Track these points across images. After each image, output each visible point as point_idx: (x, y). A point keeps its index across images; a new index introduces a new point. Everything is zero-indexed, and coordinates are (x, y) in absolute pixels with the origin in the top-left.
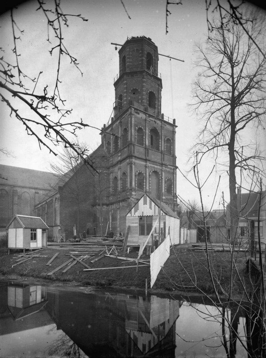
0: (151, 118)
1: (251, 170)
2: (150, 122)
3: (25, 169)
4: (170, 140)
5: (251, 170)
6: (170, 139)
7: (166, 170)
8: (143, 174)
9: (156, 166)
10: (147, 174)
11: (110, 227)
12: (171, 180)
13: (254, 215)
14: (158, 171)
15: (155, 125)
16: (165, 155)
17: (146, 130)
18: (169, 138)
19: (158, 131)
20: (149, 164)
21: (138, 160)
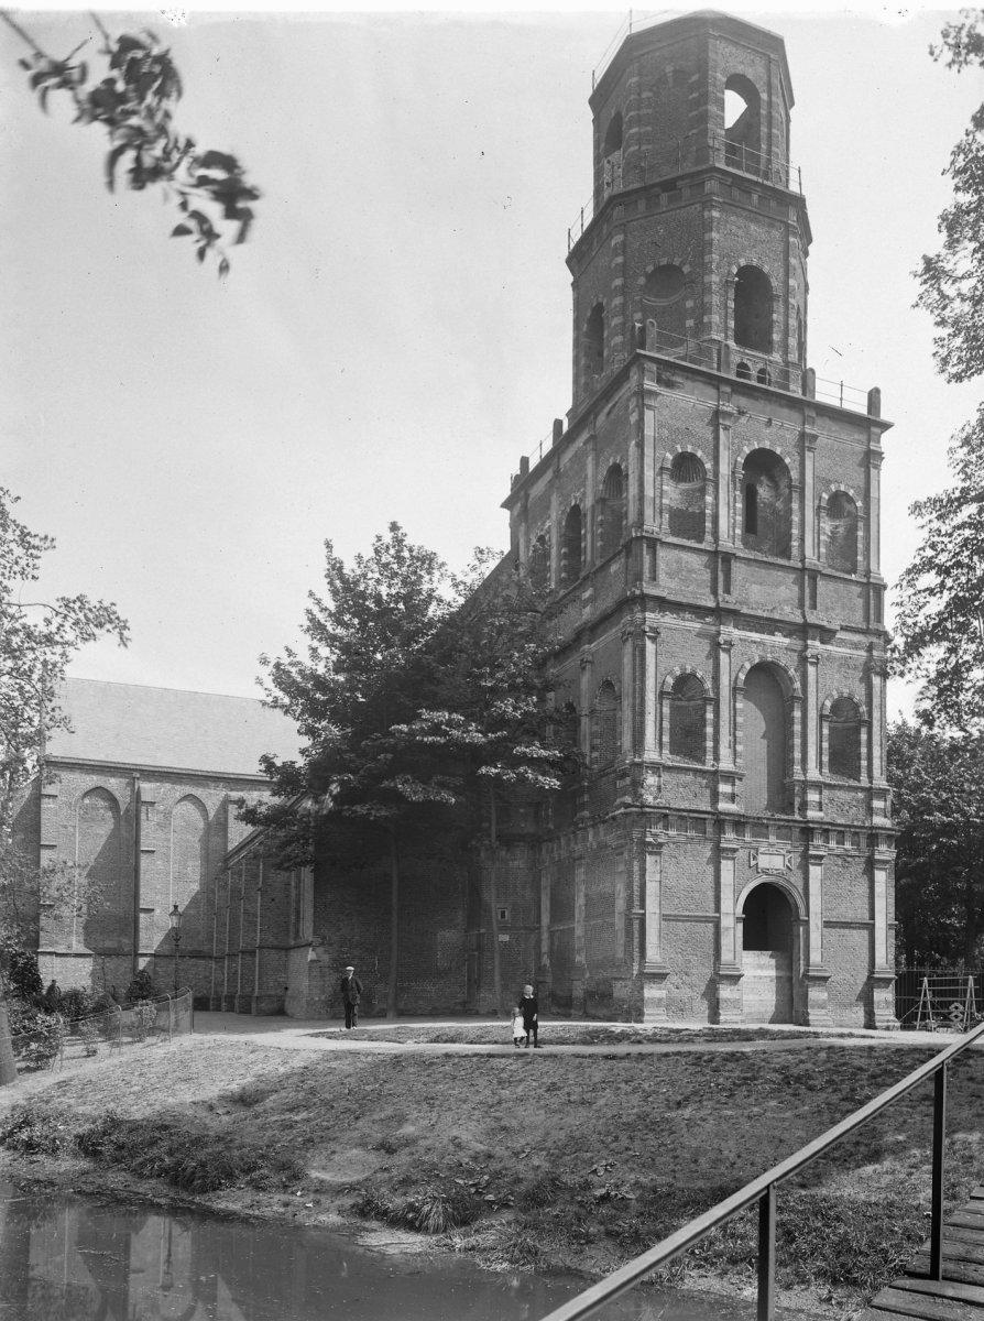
6: (851, 492)
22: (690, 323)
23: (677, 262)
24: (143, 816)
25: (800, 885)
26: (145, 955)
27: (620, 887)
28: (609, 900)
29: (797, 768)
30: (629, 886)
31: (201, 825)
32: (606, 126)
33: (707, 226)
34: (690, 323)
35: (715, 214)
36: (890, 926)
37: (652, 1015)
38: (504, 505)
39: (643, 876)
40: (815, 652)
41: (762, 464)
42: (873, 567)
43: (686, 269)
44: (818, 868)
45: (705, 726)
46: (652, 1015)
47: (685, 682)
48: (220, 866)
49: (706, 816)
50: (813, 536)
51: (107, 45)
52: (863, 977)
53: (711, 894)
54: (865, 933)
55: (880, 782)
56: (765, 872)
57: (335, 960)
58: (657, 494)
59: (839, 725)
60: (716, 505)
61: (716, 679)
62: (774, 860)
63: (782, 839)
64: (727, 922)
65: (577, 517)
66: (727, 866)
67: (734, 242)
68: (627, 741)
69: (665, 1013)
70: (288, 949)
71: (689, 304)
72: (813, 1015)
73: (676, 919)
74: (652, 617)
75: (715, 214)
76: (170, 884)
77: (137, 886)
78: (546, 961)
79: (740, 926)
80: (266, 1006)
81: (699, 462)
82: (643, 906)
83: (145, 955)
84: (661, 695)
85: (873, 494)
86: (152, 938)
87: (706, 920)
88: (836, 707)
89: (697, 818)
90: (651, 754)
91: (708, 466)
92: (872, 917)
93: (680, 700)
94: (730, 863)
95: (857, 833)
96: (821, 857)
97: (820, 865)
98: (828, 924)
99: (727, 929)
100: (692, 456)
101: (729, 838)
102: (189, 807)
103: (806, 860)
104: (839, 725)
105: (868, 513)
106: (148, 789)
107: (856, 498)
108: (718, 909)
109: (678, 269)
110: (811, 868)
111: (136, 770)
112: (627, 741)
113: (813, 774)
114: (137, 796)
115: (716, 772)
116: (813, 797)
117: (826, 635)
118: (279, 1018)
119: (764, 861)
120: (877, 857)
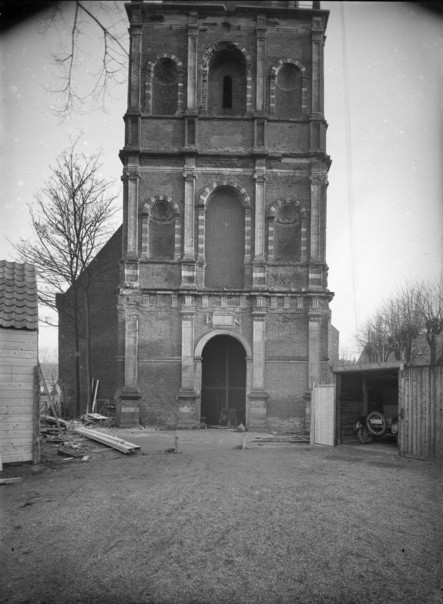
0: (210, 20)
1: (94, 234)
2: (204, 30)
3: (323, 76)
4: (297, 69)
5: (94, 234)
6: (297, 63)
7: (275, 177)
8: (172, 204)
9: (226, 171)
10: (188, 201)
11: (88, 386)
12: (299, 208)
13: (63, 336)
14: (235, 186)
15: (227, 36)
16: (266, 123)
17: (185, 61)
18: (289, 61)
19: (240, 52)
20: (192, 167)
21: (151, 164)
37: (44, 399)
40: (261, 174)
44: (261, 323)
46: (44, 399)
49: (170, 292)
51: (299, 38)
56: (219, 327)
59: (291, 225)
62: (224, 319)
63: (231, 305)
79: (199, 366)
89: (165, 295)
93: (165, 220)
94: (189, 323)
95: (295, 297)
96: (263, 315)
97: (263, 321)
103: (250, 315)
104: (291, 225)
107: (300, 66)
110: (255, 323)
111: (363, 444)
117: (271, 160)
119: (217, 320)
120: (311, 313)
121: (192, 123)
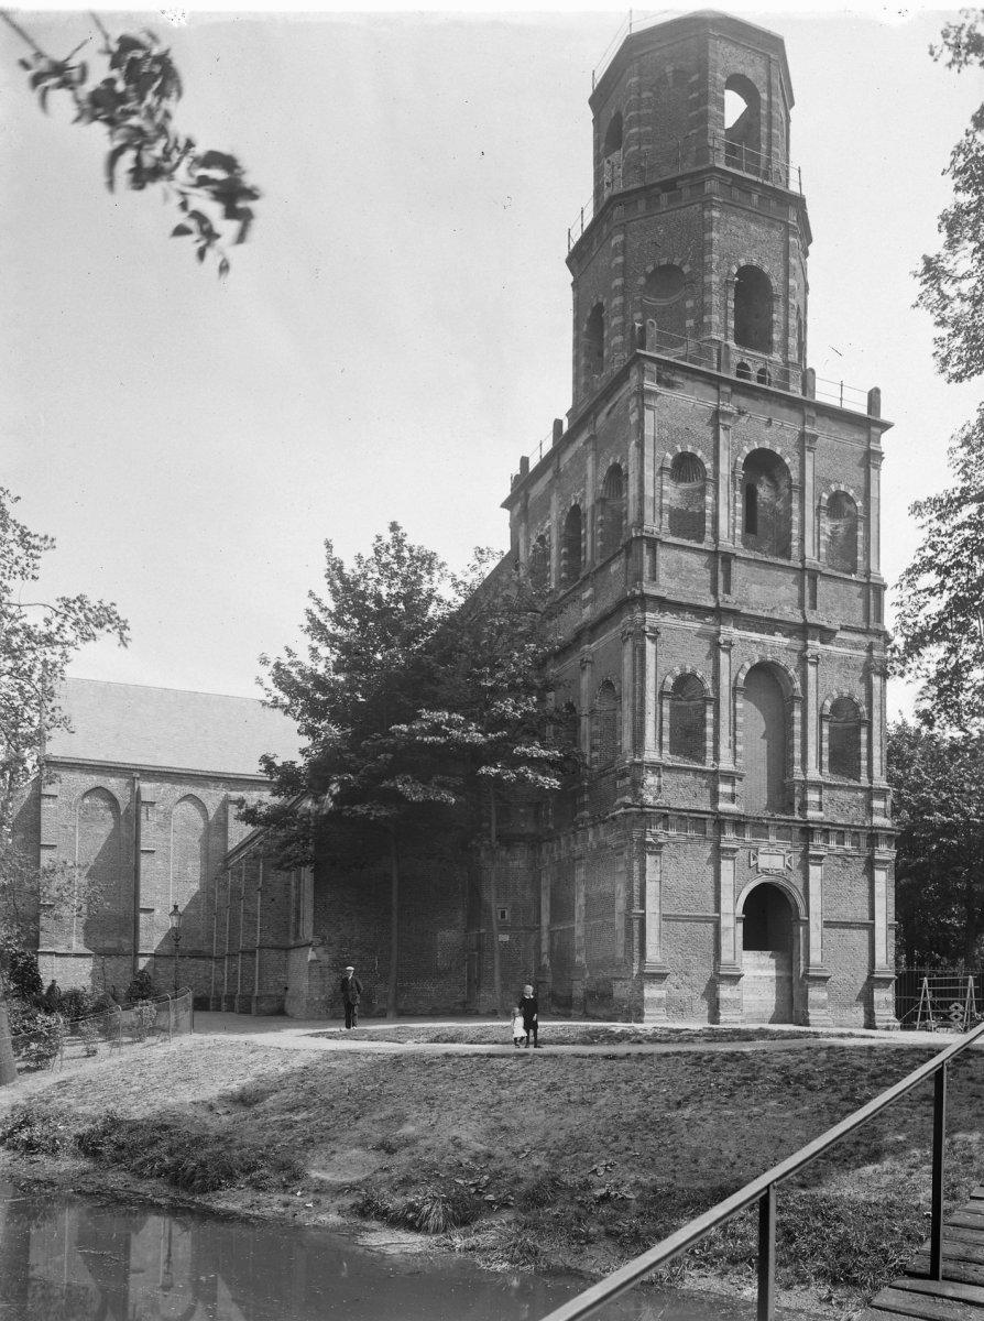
6: (851, 492)
22: (690, 323)
23: (677, 262)
24: (143, 816)
25: (800, 885)
26: (145, 955)
27: (620, 887)
28: (609, 900)
29: (797, 768)
30: (629, 886)
31: (201, 825)
32: (606, 126)
33: (707, 226)
34: (690, 323)
35: (715, 214)
36: (890, 926)
37: (652, 1015)
38: (504, 505)
39: (643, 876)
40: (815, 652)
41: (762, 464)
42: (873, 567)
43: (686, 269)
44: (818, 868)
45: (705, 726)
46: (652, 1015)
47: (685, 682)
48: (220, 866)
49: (706, 816)
50: (813, 536)
52: (863, 977)
53: (711, 894)
54: (865, 933)
55: (880, 782)
56: (765, 872)
57: (335, 960)
58: (657, 494)
59: (839, 725)
60: (716, 505)
61: (716, 679)
62: (774, 860)
63: (782, 839)
64: (727, 922)
65: (577, 517)
66: (727, 866)
67: (734, 242)
68: (627, 741)
69: (665, 1013)
70: (288, 949)
71: (689, 304)
72: (813, 1015)
73: (676, 919)
74: (652, 617)
75: (715, 214)
76: (170, 884)
77: (137, 886)
78: (546, 961)
79: (740, 926)
80: (266, 1006)
81: (699, 462)
82: (643, 906)
83: (145, 955)
84: (661, 695)
85: (873, 494)
86: (152, 938)
87: (706, 920)
88: (836, 707)
89: (697, 818)
90: (651, 754)
91: (708, 466)
92: (872, 917)
93: (680, 700)
94: (730, 863)
95: (857, 833)
96: (821, 857)
97: (820, 865)
98: (828, 924)
99: (727, 929)
100: (692, 456)
101: (729, 838)
102: (189, 807)
103: (806, 860)
104: (839, 725)
105: (868, 513)
106: (148, 789)
107: (856, 498)
108: (718, 909)
109: (678, 269)
110: (811, 868)
112: (627, 741)
113: (813, 774)
114: (137, 796)
115: (716, 772)
116: (813, 797)
117: (826, 635)
118: (279, 1018)
119: (764, 861)
120: (877, 857)
121: (814, 579)
